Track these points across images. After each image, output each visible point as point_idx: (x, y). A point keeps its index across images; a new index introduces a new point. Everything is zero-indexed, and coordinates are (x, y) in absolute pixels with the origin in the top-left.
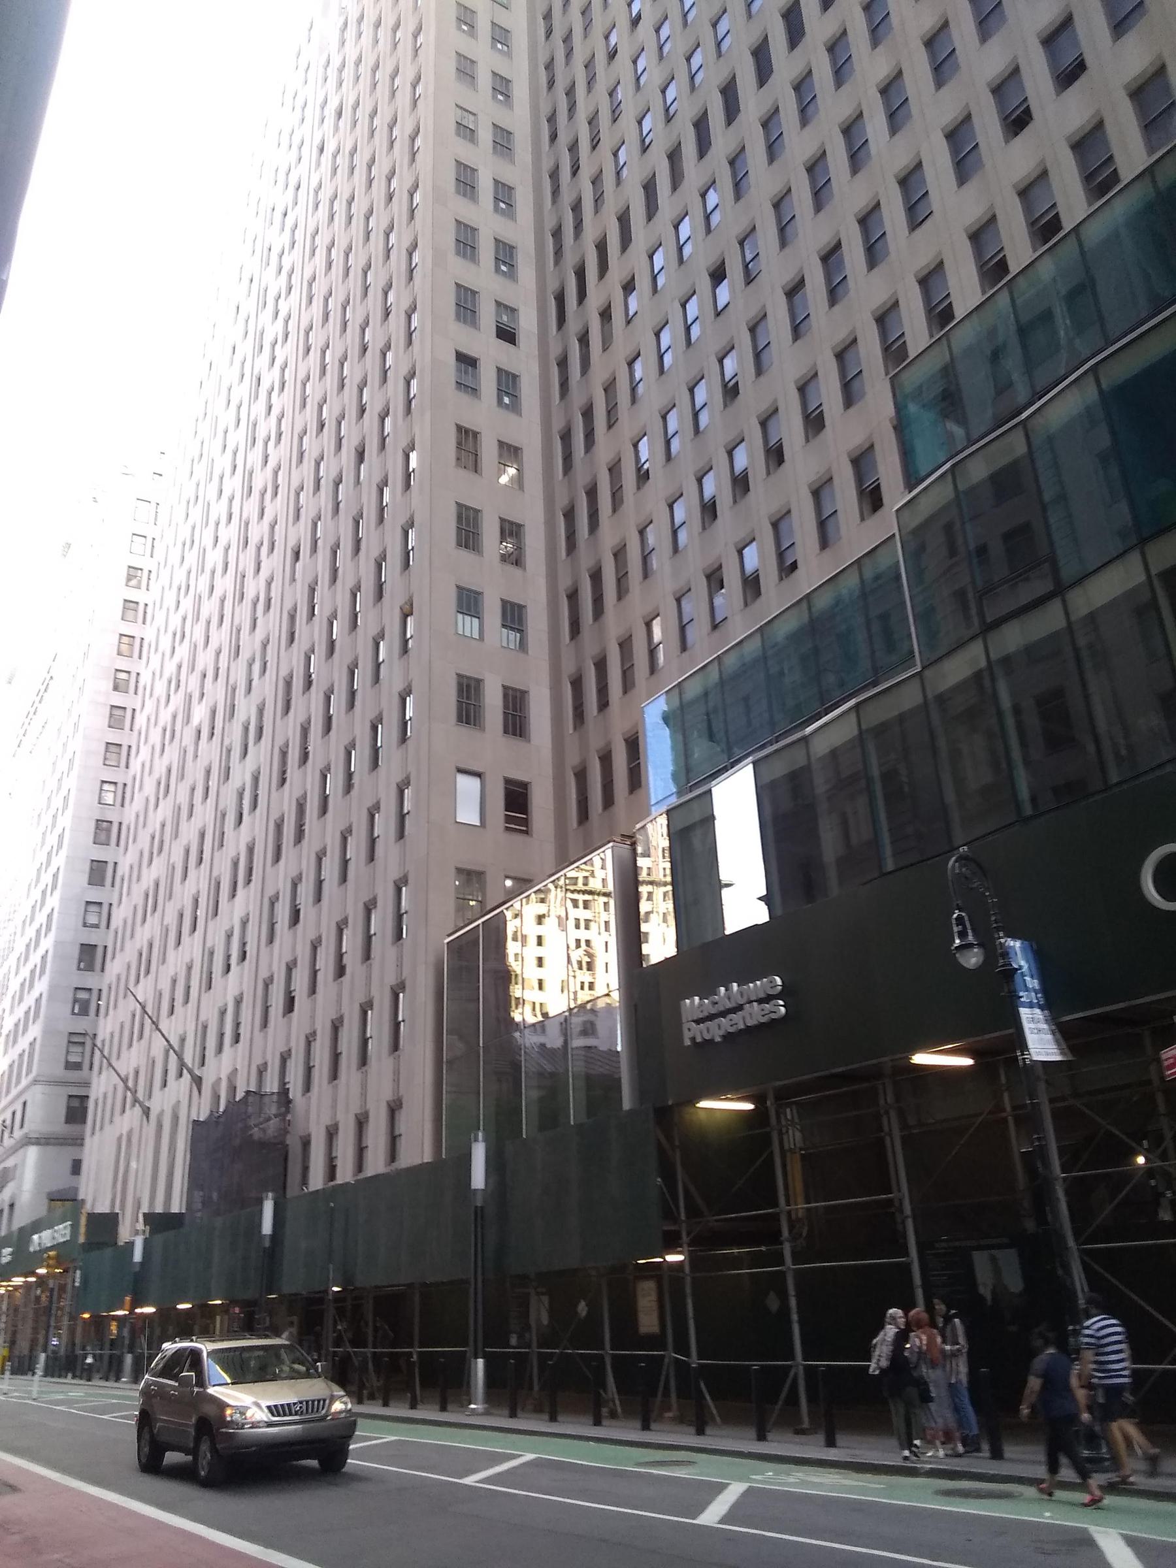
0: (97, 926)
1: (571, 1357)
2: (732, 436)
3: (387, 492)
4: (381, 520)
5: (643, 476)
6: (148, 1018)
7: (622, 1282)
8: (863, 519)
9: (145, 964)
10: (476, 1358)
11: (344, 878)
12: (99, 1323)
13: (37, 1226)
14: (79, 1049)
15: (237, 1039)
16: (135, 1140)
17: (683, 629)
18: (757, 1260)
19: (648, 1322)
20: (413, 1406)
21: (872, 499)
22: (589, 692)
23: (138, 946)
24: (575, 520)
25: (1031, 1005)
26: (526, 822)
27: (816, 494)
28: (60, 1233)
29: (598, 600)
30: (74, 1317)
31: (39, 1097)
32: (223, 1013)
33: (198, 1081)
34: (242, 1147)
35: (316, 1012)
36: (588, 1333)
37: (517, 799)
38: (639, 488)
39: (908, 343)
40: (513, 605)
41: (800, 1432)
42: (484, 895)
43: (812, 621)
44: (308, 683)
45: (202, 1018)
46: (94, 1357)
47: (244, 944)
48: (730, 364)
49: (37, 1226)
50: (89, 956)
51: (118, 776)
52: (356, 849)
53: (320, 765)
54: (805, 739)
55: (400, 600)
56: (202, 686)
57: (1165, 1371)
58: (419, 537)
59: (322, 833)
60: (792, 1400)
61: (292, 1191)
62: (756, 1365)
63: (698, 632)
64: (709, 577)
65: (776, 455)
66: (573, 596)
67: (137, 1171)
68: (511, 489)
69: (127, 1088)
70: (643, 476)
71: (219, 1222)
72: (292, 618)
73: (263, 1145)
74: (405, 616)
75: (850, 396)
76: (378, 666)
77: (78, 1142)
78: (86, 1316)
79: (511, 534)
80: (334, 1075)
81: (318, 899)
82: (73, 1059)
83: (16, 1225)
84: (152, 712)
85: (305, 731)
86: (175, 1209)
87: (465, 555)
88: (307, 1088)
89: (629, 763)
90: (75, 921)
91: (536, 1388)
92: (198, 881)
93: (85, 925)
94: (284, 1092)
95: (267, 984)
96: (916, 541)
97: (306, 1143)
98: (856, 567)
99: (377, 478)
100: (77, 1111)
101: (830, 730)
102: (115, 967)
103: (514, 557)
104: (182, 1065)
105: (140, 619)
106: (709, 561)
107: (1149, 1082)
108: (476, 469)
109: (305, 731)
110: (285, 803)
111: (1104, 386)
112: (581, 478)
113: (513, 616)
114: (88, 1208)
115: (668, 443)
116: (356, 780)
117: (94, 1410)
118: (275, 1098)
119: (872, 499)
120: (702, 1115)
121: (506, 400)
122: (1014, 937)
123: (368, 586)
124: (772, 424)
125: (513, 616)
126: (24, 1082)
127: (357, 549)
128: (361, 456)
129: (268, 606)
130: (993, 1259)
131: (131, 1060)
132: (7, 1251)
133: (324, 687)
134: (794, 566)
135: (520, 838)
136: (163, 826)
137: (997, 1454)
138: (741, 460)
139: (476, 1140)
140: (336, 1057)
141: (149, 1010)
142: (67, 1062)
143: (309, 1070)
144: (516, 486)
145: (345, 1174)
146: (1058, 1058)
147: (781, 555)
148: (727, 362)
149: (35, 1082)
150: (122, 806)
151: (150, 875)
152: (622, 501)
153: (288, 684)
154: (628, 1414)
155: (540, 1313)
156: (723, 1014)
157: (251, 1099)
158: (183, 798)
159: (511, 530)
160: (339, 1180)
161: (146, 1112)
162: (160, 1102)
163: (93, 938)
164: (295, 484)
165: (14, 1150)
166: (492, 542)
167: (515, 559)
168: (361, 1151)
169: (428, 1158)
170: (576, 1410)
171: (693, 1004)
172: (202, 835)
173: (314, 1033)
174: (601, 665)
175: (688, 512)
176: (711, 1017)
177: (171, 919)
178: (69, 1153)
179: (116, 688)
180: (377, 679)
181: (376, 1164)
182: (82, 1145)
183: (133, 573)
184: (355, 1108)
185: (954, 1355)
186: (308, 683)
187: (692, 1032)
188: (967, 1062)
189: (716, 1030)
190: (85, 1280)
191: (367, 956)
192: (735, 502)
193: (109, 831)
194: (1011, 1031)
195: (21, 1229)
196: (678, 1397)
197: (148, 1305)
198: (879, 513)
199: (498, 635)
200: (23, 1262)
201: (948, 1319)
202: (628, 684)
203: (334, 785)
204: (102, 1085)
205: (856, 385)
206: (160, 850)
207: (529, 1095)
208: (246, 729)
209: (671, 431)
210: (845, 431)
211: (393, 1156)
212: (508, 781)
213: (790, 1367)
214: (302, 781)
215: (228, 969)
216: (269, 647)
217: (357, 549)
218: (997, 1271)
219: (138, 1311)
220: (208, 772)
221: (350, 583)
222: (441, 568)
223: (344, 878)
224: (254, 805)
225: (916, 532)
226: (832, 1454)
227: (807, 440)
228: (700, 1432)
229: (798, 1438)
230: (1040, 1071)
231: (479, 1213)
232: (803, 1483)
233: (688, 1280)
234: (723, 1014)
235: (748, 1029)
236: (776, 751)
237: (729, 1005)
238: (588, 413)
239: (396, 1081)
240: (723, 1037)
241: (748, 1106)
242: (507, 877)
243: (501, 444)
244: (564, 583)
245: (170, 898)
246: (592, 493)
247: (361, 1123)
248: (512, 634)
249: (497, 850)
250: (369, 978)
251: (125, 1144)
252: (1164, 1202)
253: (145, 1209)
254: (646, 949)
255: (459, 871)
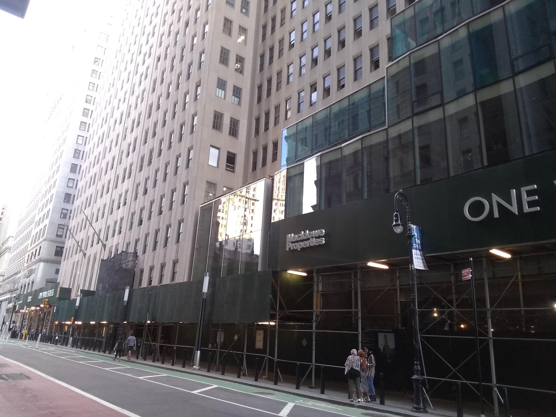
0: (72, 187)
1: (232, 354)
2: (327, 35)
3: (195, 39)
4: (192, 49)
5: (292, 46)
6: (88, 222)
7: (253, 329)
8: (371, 71)
9: (89, 202)
10: (197, 350)
11: (165, 180)
12: (61, 326)
13: (41, 290)
14: (62, 230)
15: (120, 232)
16: (80, 264)
17: (299, 104)
18: (300, 327)
19: (259, 344)
20: (173, 365)
21: (376, 64)
22: (261, 124)
23: (87, 196)
24: (264, 59)
25: (416, 249)
26: (233, 168)
27: (355, 60)
28: (51, 293)
29: (269, 90)
30: (52, 323)
31: (46, 245)
32: (116, 223)
33: (104, 246)
34: (118, 270)
35: (150, 226)
36: (238, 346)
37: (231, 159)
38: (289, 50)
39: (397, 8)
40: (238, 88)
41: (312, 388)
42: (215, 192)
43: (369, 95)
44: (158, 108)
45: (108, 224)
46: (58, 337)
47: (126, 199)
48: (330, 7)
49: (41, 290)
50: (68, 198)
51: (84, 134)
52: (170, 170)
53: (160, 138)
54: (341, 148)
55: (196, 80)
56: (119, 105)
57: (445, 381)
58: (205, 57)
59: (159, 163)
60: (310, 376)
61: (136, 286)
62: (298, 363)
63: (305, 106)
64: (311, 86)
65: (342, 44)
66: (260, 87)
67: (80, 274)
68: (242, 44)
69: (78, 245)
70: (292, 46)
71: (108, 295)
72: (155, 82)
73: (126, 270)
74: (197, 86)
75: (372, 25)
76: (185, 104)
77: (59, 263)
78: (57, 323)
79: (240, 61)
80: (155, 249)
81: (155, 186)
82: (59, 233)
83: (34, 289)
84: (99, 111)
85: (155, 125)
86: (92, 289)
87: (222, 66)
88: (144, 252)
89: (273, 151)
90: (64, 184)
91: (217, 362)
92: (111, 175)
93: (67, 186)
94: (135, 253)
95: (133, 214)
96: (395, 79)
97: (142, 271)
98: (348, 98)
99: (192, 33)
100: (59, 252)
101: (350, 146)
102: (77, 203)
103: (240, 70)
104: (99, 239)
105: (98, 77)
106: (312, 81)
107: (451, 282)
108: (230, 34)
109: (155, 125)
110: (146, 150)
111: (470, 30)
112: (268, 43)
113: (237, 92)
114: (61, 284)
115: (302, 34)
116: (173, 144)
117: (58, 355)
118: (132, 254)
119: (376, 64)
120: (288, 275)
121: (244, 10)
122: (414, 224)
123: (185, 73)
124: (342, 32)
125: (237, 92)
126: (41, 240)
127: (182, 59)
128: (187, 24)
129: (146, 78)
130: (385, 336)
131: (80, 236)
132: (30, 297)
133: (165, 109)
134: (343, 86)
135: (231, 173)
136: (100, 154)
137: (382, 403)
138: (316, 53)
139: (206, 275)
140: (156, 243)
141: (89, 218)
142: (57, 234)
143: (145, 246)
144: (244, 43)
145: (155, 283)
146: (423, 269)
147: (339, 81)
148: (329, 6)
149: (45, 240)
150: (85, 145)
151: (93, 171)
152: (282, 54)
153: (151, 107)
154: (250, 375)
155: (220, 338)
156: (302, 241)
157: (123, 254)
158: (108, 144)
159: (240, 60)
160: (153, 285)
161: (85, 255)
162: (90, 252)
163: (70, 191)
164: (161, 33)
165: (35, 263)
166: (233, 64)
167: (240, 71)
168: (161, 276)
169: (186, 280)
170: (232, 372)
171: (291, 236)
172: (114, 159)
173: (149, 234)
174: (267, 114)
175: (307, 61)
176: (297, 242)
177: (100, 187)
178: (55, 266)
179: (86, 102)
180: (184, 109)
181: (167, 280)
182: (60, 264)
183: (96, 60)
184: (161, 261)
185: (370, 367)
186: (158, 108)
187: (289, 246)
188: (386, 267)
189: (298, 246)
190: (57, 310)
191: (171, 208)
192: (325, 59)
193: (79, 154)
194: (409, 257)
195: (36, 291)
196: (268, 371)
197: (79, 321)
198: (377, 70)
199: (231, 99)
200: (36, 302)
201: (369, 355)
202: (276, 123)
203: (165, 146)
204: (69, 244)
205: (375, 21)
206: (98, 163)
207: (224, 264)
208: (134, 122)
209: (304, 30)
210: (369, 38)
211: (173, 278)
212: (229, 153)
213: (310, 365)
214: (153, 143)
215: (119, 207)
216: (145, 93)
217: (182, 59)
218: (386, 340)
219: (76, 323)
220: (118, 136)
221: (178, 72)
222: (213, 70)
223: (165, 180)
224: (134, 150)
225: (393, 77)
226: (323, 396)
227: (354, 40)
228: (276, 384)
229: (310, 390)
230: (415, 272)
231: (204, 301)
232: (313, 405)
233: (277, 331)
234: (302, 241)
235: (310, 247)
236: (330, 151)
237: (304, 238)
238: (274, 20)
239: (177, 253)
240: (301, 249)
241: (305, 274)
242: (224, 187)
243: (240, 27)
244: (257, 82)
245: (100, 180)
246: (272, 50)
247: (163, 266)
248: (236, 99)
249: (222, 177)
250: (171, 216)
251: (76, 265)
252: (447, 324)
253: (81, 288)
254: (273, 214)
255: (208, 182)
